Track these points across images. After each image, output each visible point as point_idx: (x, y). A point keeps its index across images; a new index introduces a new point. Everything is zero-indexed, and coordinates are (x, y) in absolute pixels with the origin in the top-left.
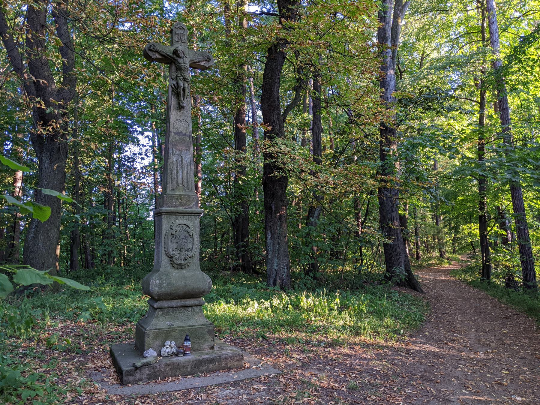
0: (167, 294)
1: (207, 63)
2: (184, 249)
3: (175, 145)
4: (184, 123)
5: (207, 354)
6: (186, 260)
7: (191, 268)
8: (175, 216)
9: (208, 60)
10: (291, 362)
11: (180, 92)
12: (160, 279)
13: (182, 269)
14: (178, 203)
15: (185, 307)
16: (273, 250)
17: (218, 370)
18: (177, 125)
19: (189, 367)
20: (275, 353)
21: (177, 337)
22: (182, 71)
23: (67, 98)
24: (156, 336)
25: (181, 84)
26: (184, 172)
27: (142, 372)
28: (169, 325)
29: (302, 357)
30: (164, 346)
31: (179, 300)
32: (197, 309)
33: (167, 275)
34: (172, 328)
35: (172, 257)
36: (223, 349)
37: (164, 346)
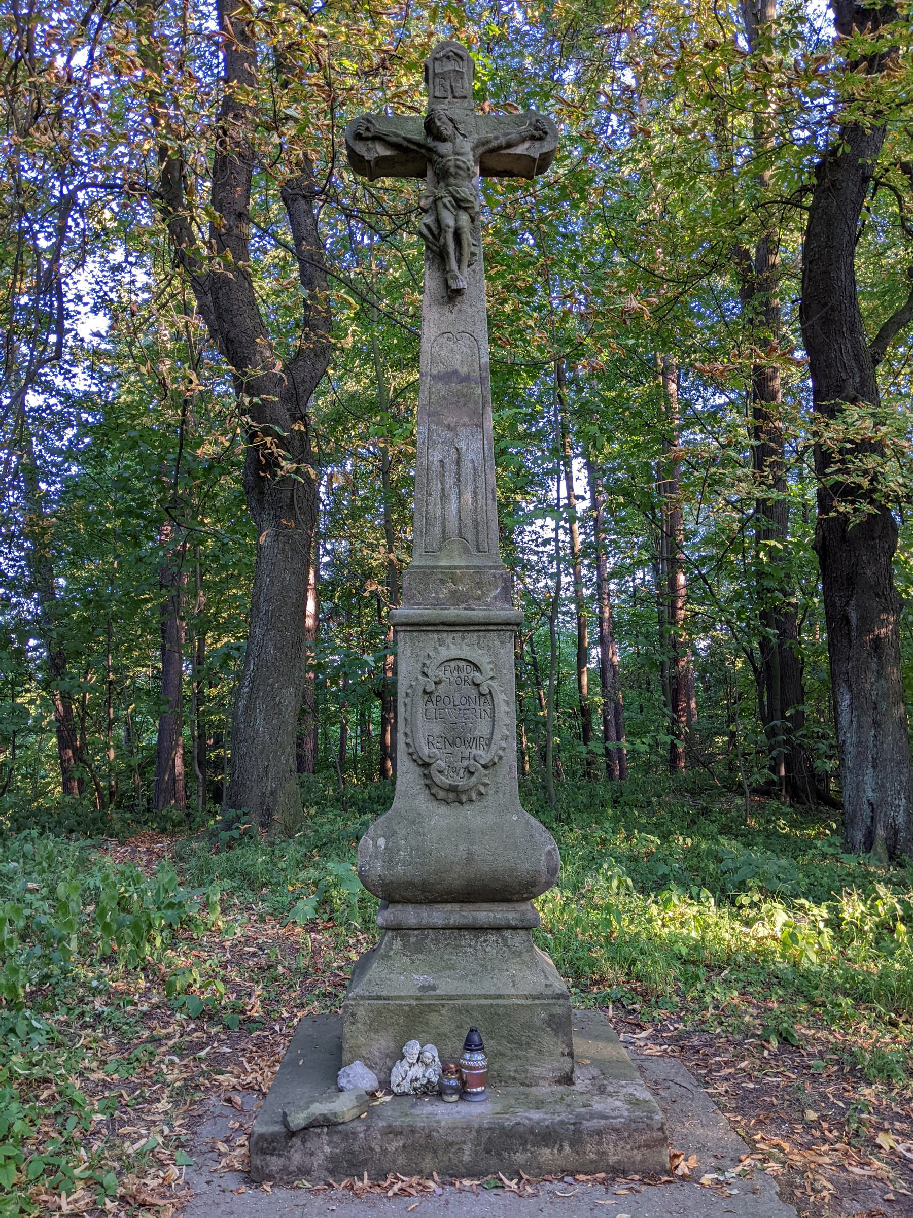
0: (410, 884)
1: (537, 144)
2: (463, 741)
3: (435, 414)
4: (464, 344)
5: (539, 1104)
6: (473, 773)
7: (490, 801)
8: (435, 636)
9: (536, 133)
10: (867, 1171)
11: (445, 245)
12: (390, 835)
13: (461, 803)
14: (444, 593)
15: (478, 929)
16: (859, 743)
17: (572, 1174)
18: (443, 353)
19: (467, 1149)
20: (812, 1115)
21: (445, 1029)
22: (452, 180)
24: (377, 1023)
25: (448, 219)
27: (308, 1145)
28: (423, 988)
30: (403, 1057)
31: (456, 907)
32: (517, 940)
33: (413, 822)
34: (431, 997)
35: (426, 765)
36: (602, 1090)
37: (403, 1057)
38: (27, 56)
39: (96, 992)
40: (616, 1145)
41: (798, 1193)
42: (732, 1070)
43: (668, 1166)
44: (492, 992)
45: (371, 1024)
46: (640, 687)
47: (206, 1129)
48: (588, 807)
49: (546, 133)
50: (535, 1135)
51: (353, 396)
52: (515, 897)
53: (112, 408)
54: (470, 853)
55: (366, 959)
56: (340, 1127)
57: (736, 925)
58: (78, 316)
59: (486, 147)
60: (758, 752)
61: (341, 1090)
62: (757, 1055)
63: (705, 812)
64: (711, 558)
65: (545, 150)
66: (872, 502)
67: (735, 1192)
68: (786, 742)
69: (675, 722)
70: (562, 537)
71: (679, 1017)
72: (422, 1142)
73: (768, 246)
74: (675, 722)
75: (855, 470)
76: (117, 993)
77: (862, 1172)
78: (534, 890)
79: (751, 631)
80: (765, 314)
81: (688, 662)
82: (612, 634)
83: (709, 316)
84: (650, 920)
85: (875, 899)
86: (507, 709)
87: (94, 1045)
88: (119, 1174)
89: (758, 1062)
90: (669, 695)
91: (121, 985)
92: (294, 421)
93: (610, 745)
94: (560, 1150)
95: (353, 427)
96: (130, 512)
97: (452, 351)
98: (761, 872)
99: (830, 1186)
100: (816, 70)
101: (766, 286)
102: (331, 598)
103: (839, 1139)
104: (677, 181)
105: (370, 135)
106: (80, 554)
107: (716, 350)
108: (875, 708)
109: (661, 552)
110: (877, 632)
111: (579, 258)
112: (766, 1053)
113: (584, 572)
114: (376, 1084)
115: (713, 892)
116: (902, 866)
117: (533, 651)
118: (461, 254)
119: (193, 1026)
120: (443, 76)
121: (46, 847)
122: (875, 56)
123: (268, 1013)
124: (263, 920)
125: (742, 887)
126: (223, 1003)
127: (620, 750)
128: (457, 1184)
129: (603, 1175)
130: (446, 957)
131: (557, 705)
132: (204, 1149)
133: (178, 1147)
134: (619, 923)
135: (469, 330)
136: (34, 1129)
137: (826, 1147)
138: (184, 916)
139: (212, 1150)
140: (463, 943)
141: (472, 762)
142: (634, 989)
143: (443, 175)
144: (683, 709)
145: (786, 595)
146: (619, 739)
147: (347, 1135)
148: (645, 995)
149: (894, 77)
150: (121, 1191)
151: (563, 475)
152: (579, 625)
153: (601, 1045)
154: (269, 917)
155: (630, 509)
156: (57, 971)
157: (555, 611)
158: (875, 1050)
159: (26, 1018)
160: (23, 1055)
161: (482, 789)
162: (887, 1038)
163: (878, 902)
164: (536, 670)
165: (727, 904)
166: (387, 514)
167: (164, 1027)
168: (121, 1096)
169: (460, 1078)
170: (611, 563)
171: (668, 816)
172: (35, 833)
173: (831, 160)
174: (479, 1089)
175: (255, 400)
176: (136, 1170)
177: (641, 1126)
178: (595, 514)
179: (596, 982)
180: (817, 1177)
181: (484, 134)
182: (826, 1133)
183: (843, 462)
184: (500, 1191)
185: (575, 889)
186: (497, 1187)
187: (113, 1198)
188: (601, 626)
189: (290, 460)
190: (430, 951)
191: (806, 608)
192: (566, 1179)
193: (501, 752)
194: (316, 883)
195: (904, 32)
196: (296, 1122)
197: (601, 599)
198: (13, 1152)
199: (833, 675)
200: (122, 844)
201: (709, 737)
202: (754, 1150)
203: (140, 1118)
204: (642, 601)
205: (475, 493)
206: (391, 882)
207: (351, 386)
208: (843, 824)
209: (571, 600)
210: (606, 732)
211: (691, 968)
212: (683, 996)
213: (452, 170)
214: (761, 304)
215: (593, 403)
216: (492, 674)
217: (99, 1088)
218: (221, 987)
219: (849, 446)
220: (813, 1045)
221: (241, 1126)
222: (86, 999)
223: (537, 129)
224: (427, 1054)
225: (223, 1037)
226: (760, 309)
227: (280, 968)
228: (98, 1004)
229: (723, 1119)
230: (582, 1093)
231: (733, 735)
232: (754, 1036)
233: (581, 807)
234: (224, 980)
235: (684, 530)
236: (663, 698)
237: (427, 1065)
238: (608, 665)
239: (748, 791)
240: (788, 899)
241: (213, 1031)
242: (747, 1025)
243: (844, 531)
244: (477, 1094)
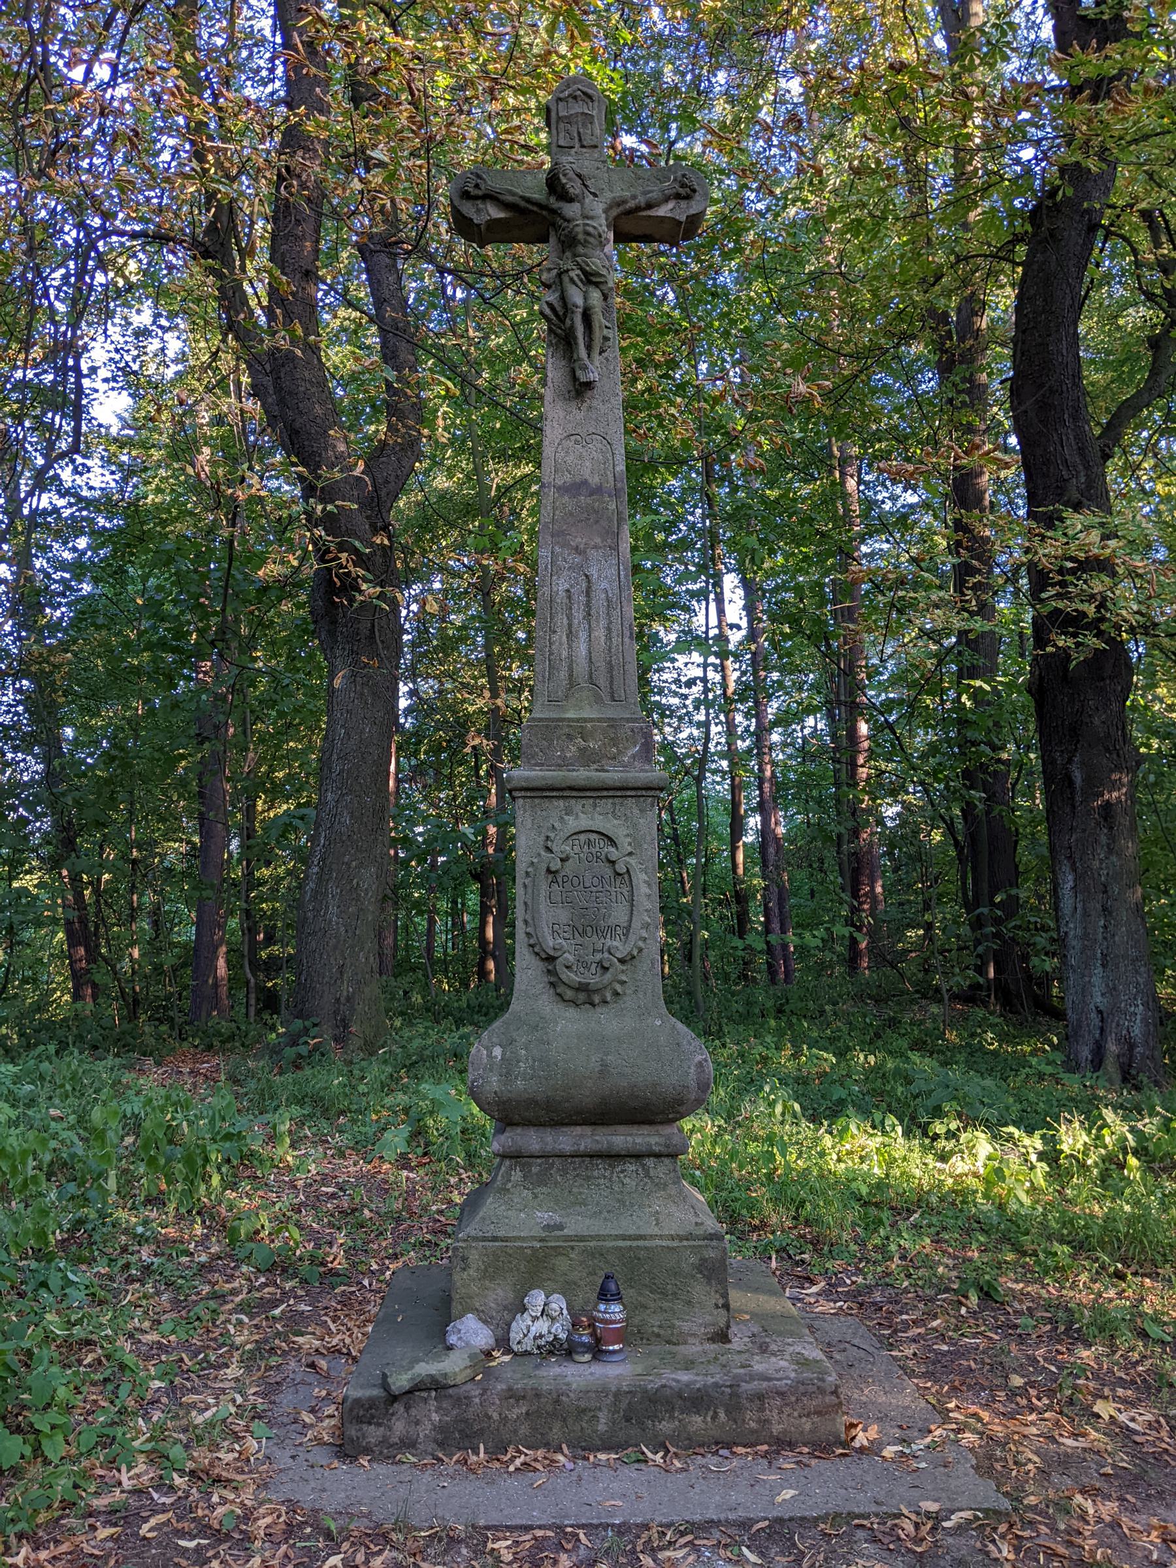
0: (532, 1103)
1: (683, 204)
2: (596, 930)
4: (597, 445)
5: (689, 1365)
6: (606, 969)
7: (629, 1002)
8: (561, 803)
10: (1081, 1443)
11: (572, 328)
12: (508, 1043)
13: (593, 1005)
14: (572, 751)
15: (613, 1157)
16: (1085, 936)
17: (728, 1446)
18: (570, 459)
19: (603, 1417)
20: (1017, 1381)
22: (580, 250)
23: (392, 478)
24: (491, 1272)
25: (576, 296)
26: (595, 634)
27: (413, 1412)
28: (548, 1227)
29: (1139, 1419)
30: (524, 1309)
31: (588, 1130)
32: (660, 1169)
34: (558, 1238)
35: (550, 959)
36: (764, 1349)
37: (524, 1309)
38: (41, 75)
39: (141, 1240)
40: (781, 1412)
41: (998, 1466)
42: (922, 1330)
43: (843, 1436)
44: (631, 1232)
45: (486, 1270)
46: (810, 866)
47: (286, 1399)
48: (745, 1018)
49: (694, 191)
50: (684, 1399)
51: (443, 495)
52: (659, 1118)
53: (137, 511)
54: (604, 1065)
55: (473, 1202)
56: (451, 1391)
57: (930, 1159)
58: (95, 395)
59: (621, 208)
60: (960, 949)
61: (450, 1348)
62: (952, 1313)
63: (893, 1023)
64: (900, 702)
65: (692, 212)
66: (1100, 634)
67: (923, 1465)
68: (997, 935)
69: (854, 910)
70: (711, 674)
71: (858, 1269)
72: (550, 1408)
73: (973, 306)
74: (854, 910)
75: (1078, 595)
76: (167, 1240)
77: (1076, 1444)
78: (682, 1109)
79: (951, 795)
80: (968, 392)
81: (873, 834)
82: (775, 799)
83: (899, 391)
84: (822, 1154)
85: (1101, 1128)
86: (648, 891)
87: (144, 1303)
88: (187, 1447)
89: (953, 1320)
90: (848, 875)
91: (171, 1232)
92: (375, 531)
93: (772, 938)
94: (714, 1418)
95: (445, 536)
96: (163, 645)
97: (581, 457)
98: (960, 1094)
99: (1036, 1459)
100: (1028, 100)
101: (969, 358)
102: (416, 753)
103: (1049, 1408)
104: (856, 227)
105: (480, 193)
106: (94, 697)
107: (906, 437)
108: (1105, 892)
109: (838, 694)
110: (1107, 797)
111: (733, 323)
112: (963, 1311)
113: (739, 718)
114: (492, 1341)
115: (901, 1122)
116: (1138, 1088)
117: (673, 820)
118: (591, 340)
119: (263, 1280)
120: (569, 120)
121: (69, 1065)
122: (1102, 80)
123: (354, 1265)
124: (342, 1155)
125: (937, 1113)
126: (298, 1253)
127: (785, 946)
128: (592, 1458)
129: (765, 1447)
130: (575, 1190)
131: (704, 890)
132: (285, 1420)
133: (253, 1418)
134: (784, 1156)
135: (601, 431)
136: (79, 1397)
137: (1033, 1417)
138: (245, 1149)
139: (295, 1422)
140: (596, 1173)
141: (606, 955)
142: (803, 1236)
143: (569, 243)
144: (866, 894)
145: (995, 748)
146: (784, 932)
147: (459, 1399)
148: (816, 1243)
149: (1123, 112)
150: (190, 1465)
151: (712, 596)
152: (733, 786)
153: (762, 1298)
154: (349, 1151)
155: (797, 640)
156: (93, 1215)
157: (702, 770)
158: (1098, 1309)
159: (60, 1270)
160: (58, 1313)
161: (619, 988)
162: (1111, 1293)
163: (1105, 1131)
164: (677, 845)
165: (918, 1132)
166: (487, 646)
167: (227, 1282)
168: (182, 1360)
169: (593, 1334)
170: (772, 709)
171: (845, 1028)
172: (52, 1048)
173: (1049, 203)
174: (616, 1347)
175: (329, 507)
176: (207, 1442)
177: (811, 1388)
178: (753, 647)
179: (755, 1228)
180: (1021, 1449)
181: (620, 191)
182: (1034, 1400)
183: (1063, 584)
184: (642, 1466)
185: (729, 1117)
186: (638, 1461)
187: (181, 1472)
188: (760, 788)
189: (370, 581)
190: (556, 1183)
191: (1020, 766)
192: (721, 1452)
193: (641, 944)
194: (406, 1110)
195: (1137, 53)
196: (399, 1384)
197: (760, 755)
198: (61, 1420)
199: (1052, 848)
200: (159, 1064)
201: (898, 932)
202: (946, 1419)
203: (206, 1386)
204: (813, 757)
205: (609, 629)
206: (509, 1100)
207: (441, 482)
208: (1067, 1038)
209: (722, 756)
210: (767, 925)
211: (873, 1211)
212: (863, 1244)
213: (581, 237)
214: (964, 380)
215: (750, 507)
216: (630, 849)
217: (154, 1351)
218: (296, 1234)
219: (1069, 565)
220: (1021, 1302)
221: (328, 1394)
222: (131, 1249)
223: (683, 186)
224: (554, 1306)
225: (300, 1292)
226: (961, 387)
227: (366, 1212)
228: (145, 1254)
229: (910, 1384)
230: (739, 1352)
231: (929, 927)
232: (947, 1290)
233: (736, 1017)
234: (298, 1225)
235: (866, 667)
236: (840, 880)
237: (553, 1319)
238: (770, 838)
239: (946, 997)
240: (993, 1128)
241: (288, 1286)
242: (941, 1278)
243: (1066, 669)
244: (614, 1352)
